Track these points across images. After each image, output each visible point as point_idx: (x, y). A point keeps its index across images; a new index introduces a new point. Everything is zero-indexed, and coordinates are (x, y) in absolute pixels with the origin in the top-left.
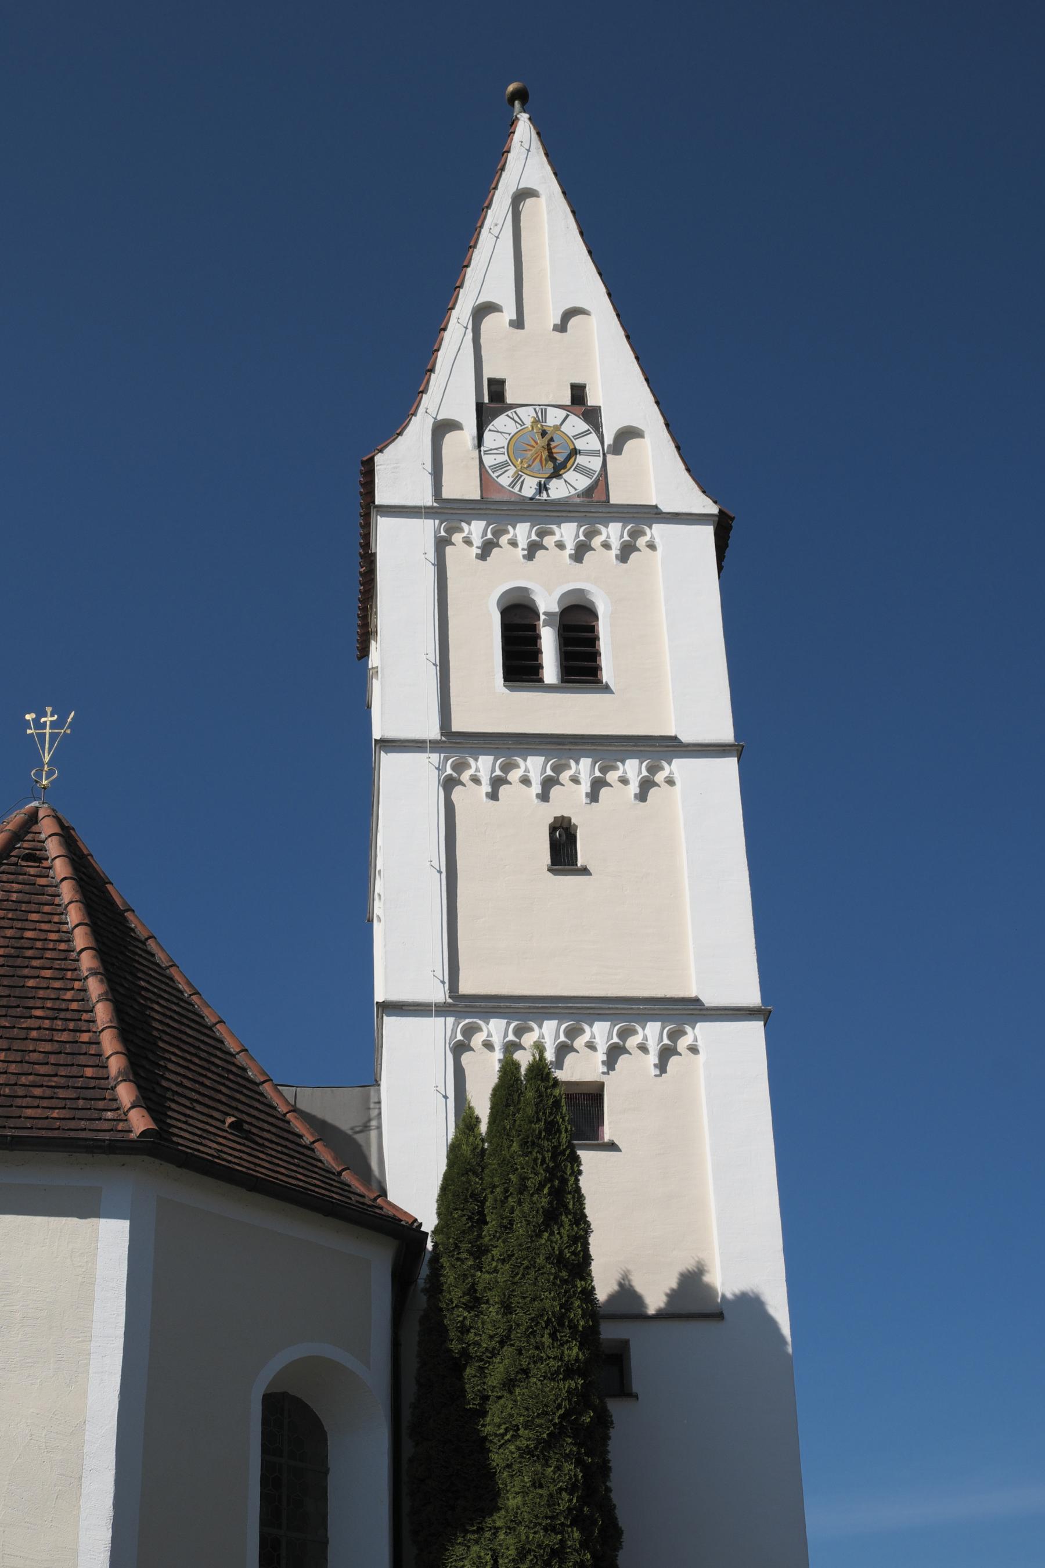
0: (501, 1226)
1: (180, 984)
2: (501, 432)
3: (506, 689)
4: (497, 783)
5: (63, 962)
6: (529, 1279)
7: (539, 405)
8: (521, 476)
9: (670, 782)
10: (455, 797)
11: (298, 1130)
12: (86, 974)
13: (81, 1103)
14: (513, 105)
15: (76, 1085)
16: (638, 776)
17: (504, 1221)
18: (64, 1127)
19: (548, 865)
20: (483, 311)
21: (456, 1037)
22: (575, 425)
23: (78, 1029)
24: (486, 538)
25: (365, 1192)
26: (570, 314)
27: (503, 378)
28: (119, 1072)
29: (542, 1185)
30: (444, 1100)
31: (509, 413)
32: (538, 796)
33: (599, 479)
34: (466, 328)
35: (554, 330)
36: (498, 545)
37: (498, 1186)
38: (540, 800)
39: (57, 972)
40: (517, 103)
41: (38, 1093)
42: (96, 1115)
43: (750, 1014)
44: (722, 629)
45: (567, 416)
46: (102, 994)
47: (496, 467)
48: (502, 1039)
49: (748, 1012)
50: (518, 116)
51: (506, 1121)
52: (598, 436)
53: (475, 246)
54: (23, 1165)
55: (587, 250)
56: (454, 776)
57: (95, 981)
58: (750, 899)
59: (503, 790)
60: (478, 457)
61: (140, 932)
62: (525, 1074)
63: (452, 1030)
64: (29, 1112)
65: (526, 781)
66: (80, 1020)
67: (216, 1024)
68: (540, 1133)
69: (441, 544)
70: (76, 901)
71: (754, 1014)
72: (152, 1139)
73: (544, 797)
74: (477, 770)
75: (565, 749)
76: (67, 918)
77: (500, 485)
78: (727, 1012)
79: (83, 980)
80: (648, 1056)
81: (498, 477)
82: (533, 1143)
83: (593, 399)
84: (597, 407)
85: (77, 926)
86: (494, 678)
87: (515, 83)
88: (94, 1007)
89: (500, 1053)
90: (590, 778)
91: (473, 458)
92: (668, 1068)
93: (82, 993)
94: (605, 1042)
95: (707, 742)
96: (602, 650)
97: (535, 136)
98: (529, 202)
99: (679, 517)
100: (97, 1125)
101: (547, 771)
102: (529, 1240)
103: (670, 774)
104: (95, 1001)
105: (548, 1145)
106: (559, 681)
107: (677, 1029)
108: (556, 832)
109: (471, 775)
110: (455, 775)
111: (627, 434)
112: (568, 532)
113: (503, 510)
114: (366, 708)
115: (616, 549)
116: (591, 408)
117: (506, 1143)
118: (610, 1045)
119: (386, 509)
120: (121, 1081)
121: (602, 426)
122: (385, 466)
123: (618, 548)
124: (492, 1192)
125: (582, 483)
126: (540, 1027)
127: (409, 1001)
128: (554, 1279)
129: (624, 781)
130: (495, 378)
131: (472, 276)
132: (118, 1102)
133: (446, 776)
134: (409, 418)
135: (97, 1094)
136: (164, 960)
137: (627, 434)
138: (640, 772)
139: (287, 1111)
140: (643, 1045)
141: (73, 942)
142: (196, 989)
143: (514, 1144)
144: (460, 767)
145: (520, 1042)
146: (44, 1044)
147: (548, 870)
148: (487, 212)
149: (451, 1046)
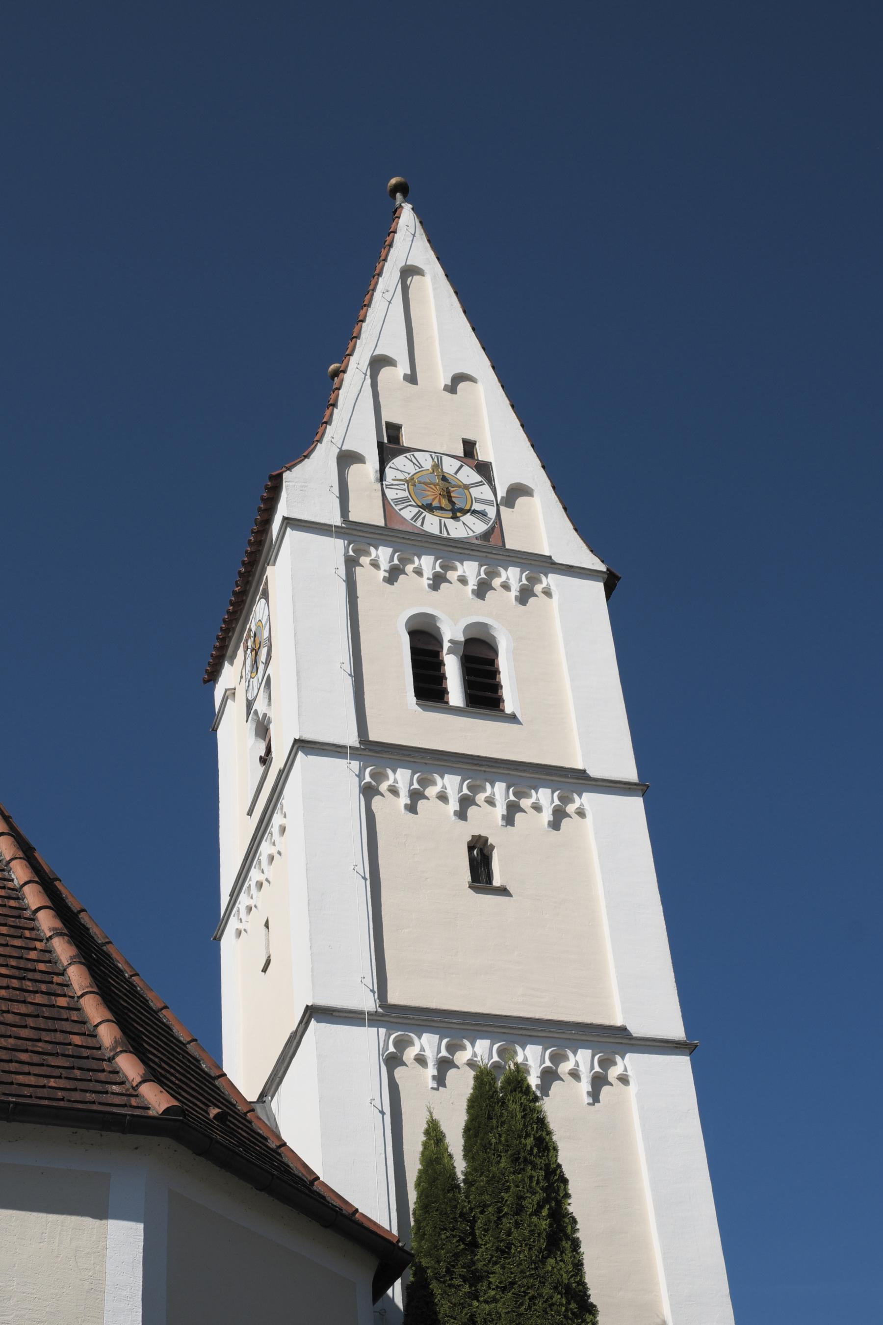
0: (498, 1249)
1: (120, 963)
2: (401, 471)
3: (418, 708)
4: (416, 796)
5: (18, 920)
6: (536, 1310)
7: (435, 453)
8: (422, 513)
9: (581, 813)
10: (374, 806)
11: (261, 1132)
12: (49, 934)
13: (77, 1073)
14: (394, 198)
15: (67, 1053)
16: (551, 805)
17: (502, 1245)
18: (69, 1098)
19: (468, 882)
20: (379, 363)
21: (387, 1049)
22: (469, 475)
23: (53, 992)
24: (392, 563)
25: (342, 1206)
26: (459, 379)
27: (399, 423)
28: (116, 1041)
29: (540, 1207)
30: (381, 1115)
31: (407, 455)
32: (456, 813)
33: (495, 526)
34: (366, 374)
35: (444, 389)
36: (403, 572)
37: (490, 1205)
38: (457, 818)
39: (12, 929)
40: (399, 196)
41: (25, 1058)
42: (99, 1087)
43: (677, 1047)
44: (618, 676)
45: (461, 466)
46: (74, 956)
47: (398, 501)
48: (435, 1054)
49: (675, 1045)
50: (403, 205)
51: (491, 1135)
52: (491, 488)
53: (369, 305)
54: (16, 1140)
55: (471, 326)
56: (373, 784)
57: (62, 942)
58: (665, 934)
59: (421, 804)
60: (380, 489)
61: (72, 904)
62: (501, 1086)
63: (384, 1041)
64: (21, 1079)
65: (443, 797)
66: (52, 983)
67: (162, 1009)
68: (532, 1149)
69: (351, 563)
70: (20, 858)
71: (680, 1048)
72: (181, 1118)
73: (462, 815)
74: (396, 781)
75: (481, 771)
76: (10, 875)
77: (403, 517)
78: (655, 1044)
79: (45, 941)
80: (580, 1084)
81: (400, 510)
82: (525, 1160)
83: (483, 454)
84: (488, 462)
85: (26, 883)
86: (406, 696)
87: (398, 178)
88: (65, 970)
89: (434, 1069)
90: (505, 801)
91: (375, 490)
92: (601, 1098)
93: (48, 955)
94: (539, 1065)
95: (613, 779)
97: (418, 224)
98: (416, 278)
99: (573, 570)
100: (104, 1098)
101: (463, 790)
102: (533, 1267)
103: (580, 806)
104: (66, 963)
105: (541, 1162)
106: (464, 704)
107: (606, 1057)
108: (474, 850)
109: (390, 786)
110: (374, 783)
111: (517, 491)
112: (470, 569)
113: (409, 539)
114: (211, 730)
115: (516, 591)
116: (482, 463)
117: (494, 1159)
118: (543, 1068)
119: (296, 523)
120: (121, 1052)
121: (494, 480)
122: (294, 484)
123: (518, 590)
124: (482, 1212)
125: (479, 527)
126: (473, 1045)
127: (338, 1007)
128: (565, 1311)
129: (537, 808)
130: (392, 423)
132: (121, 1075)
133: (365, 783)
134: (314, 445)
135: (94, 1065)
136: (99, 936)
137: (517, 491)
138: (552, 801)
139: (248, 1110)
140: (574, 1072)
141: (23, 900)
142: (135, 971)
143: (503, 1160)
144: (378, 776)
145: (453, 1059)
146: (16, 1005)
147: (469, 887)
148: (378, 279)
149: (384, 1058)
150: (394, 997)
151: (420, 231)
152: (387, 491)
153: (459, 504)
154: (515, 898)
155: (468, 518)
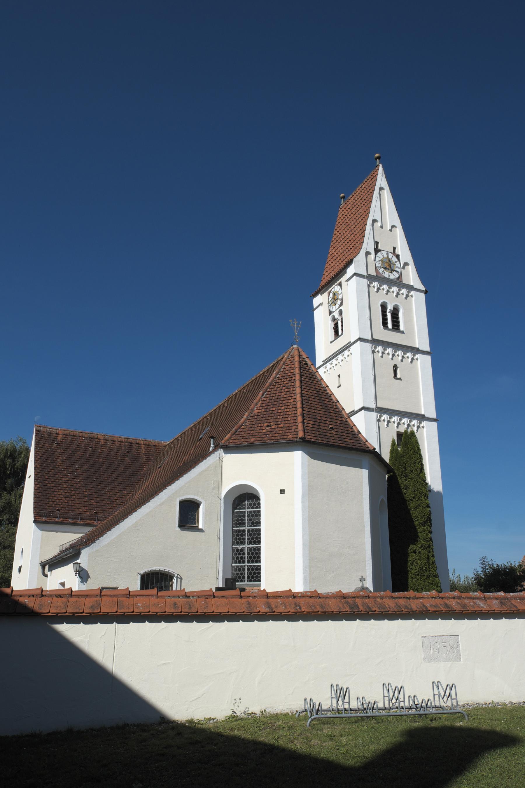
14: (377, 160)
20: (374, 221)
31: (381, 252)
47: (379, 267)
96: (400, 317)
98: (382, 191)
112: (395, 289)
125: (397, 275)
131: (364, 245)
137: (406, 264)
150: (379, 405)
151: (384, 174)
152: (376, 264)
153: (392, 268)
154: (402, 381)
155: (394, 273)
